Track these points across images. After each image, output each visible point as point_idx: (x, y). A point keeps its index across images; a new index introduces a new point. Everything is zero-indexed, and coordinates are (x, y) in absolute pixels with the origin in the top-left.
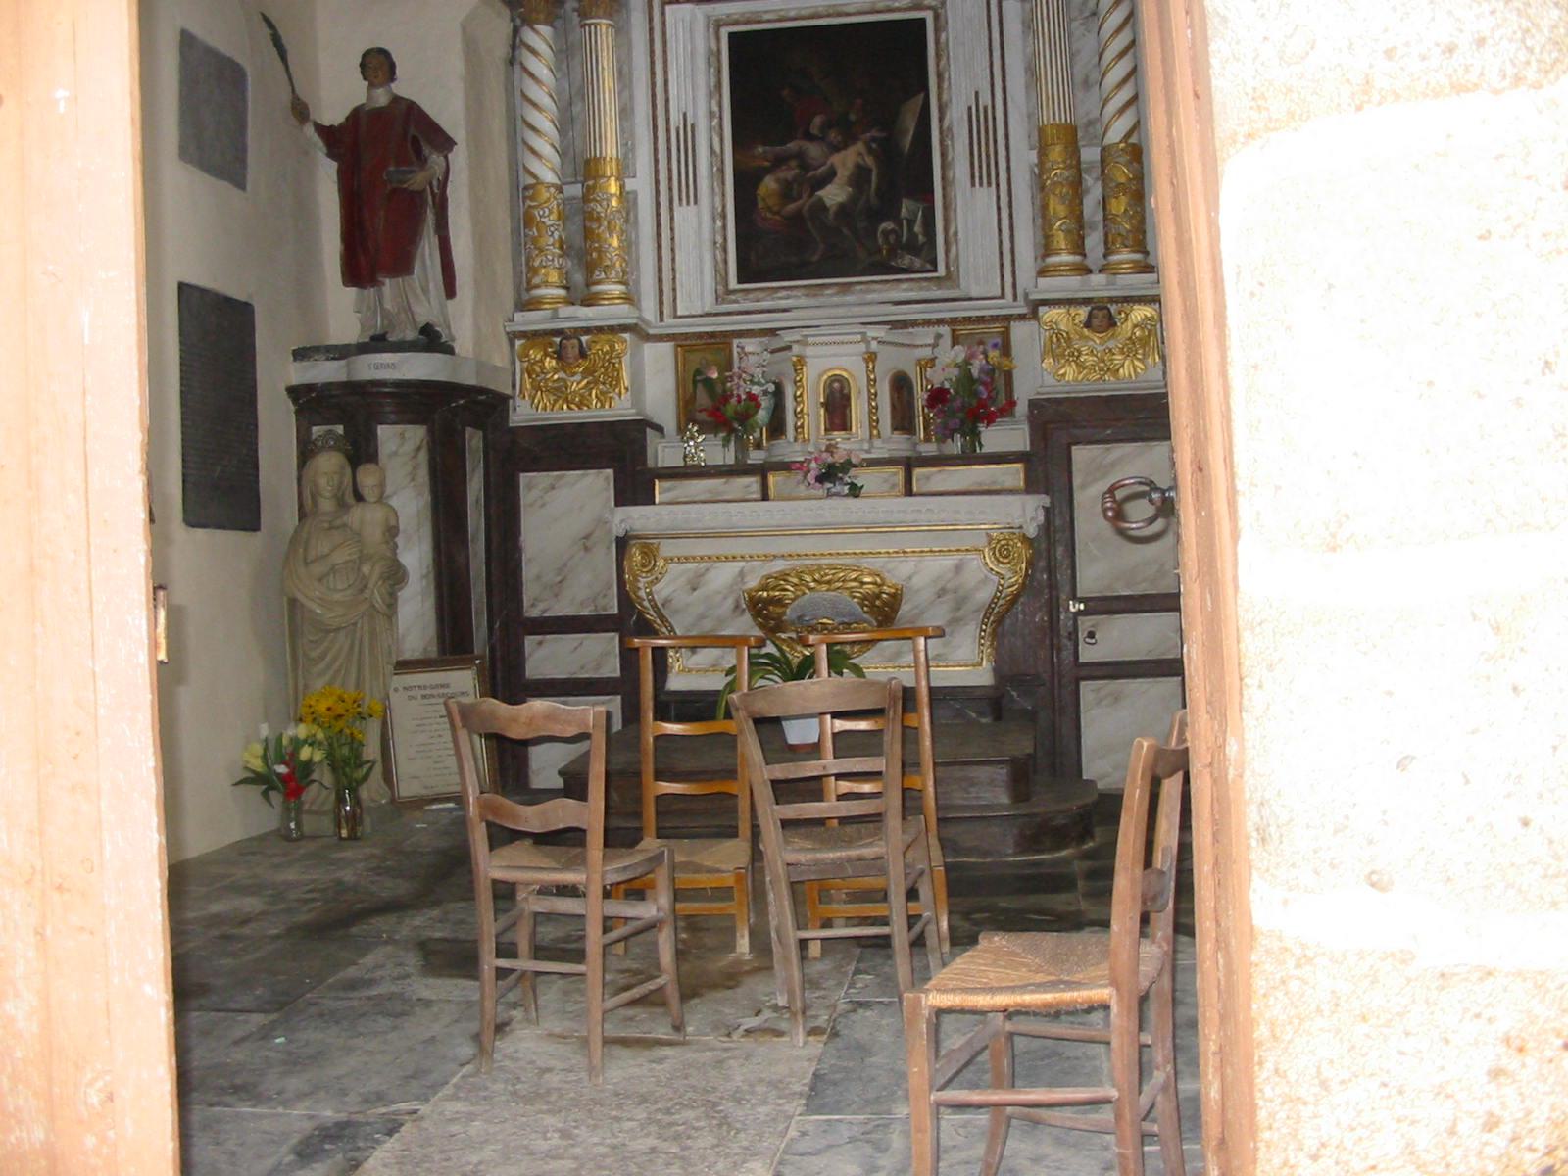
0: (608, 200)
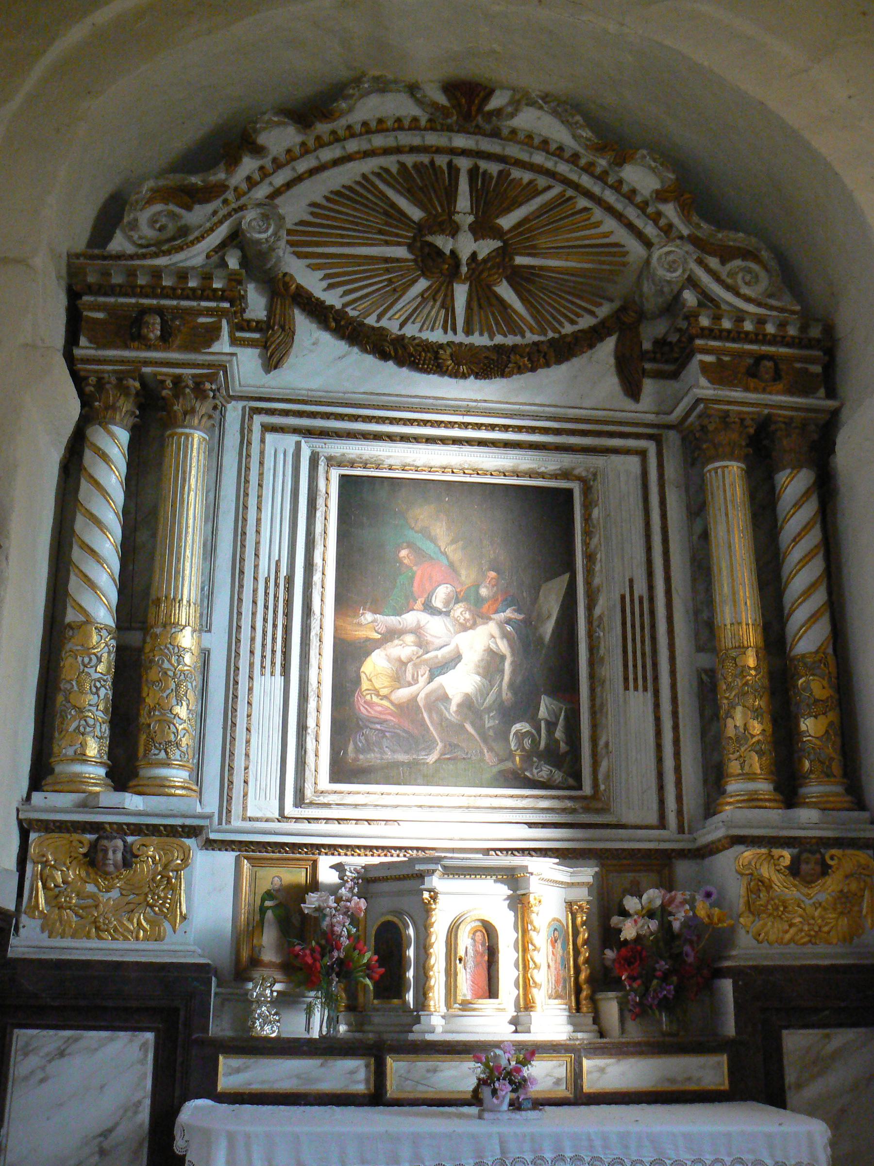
0: (180, 657)
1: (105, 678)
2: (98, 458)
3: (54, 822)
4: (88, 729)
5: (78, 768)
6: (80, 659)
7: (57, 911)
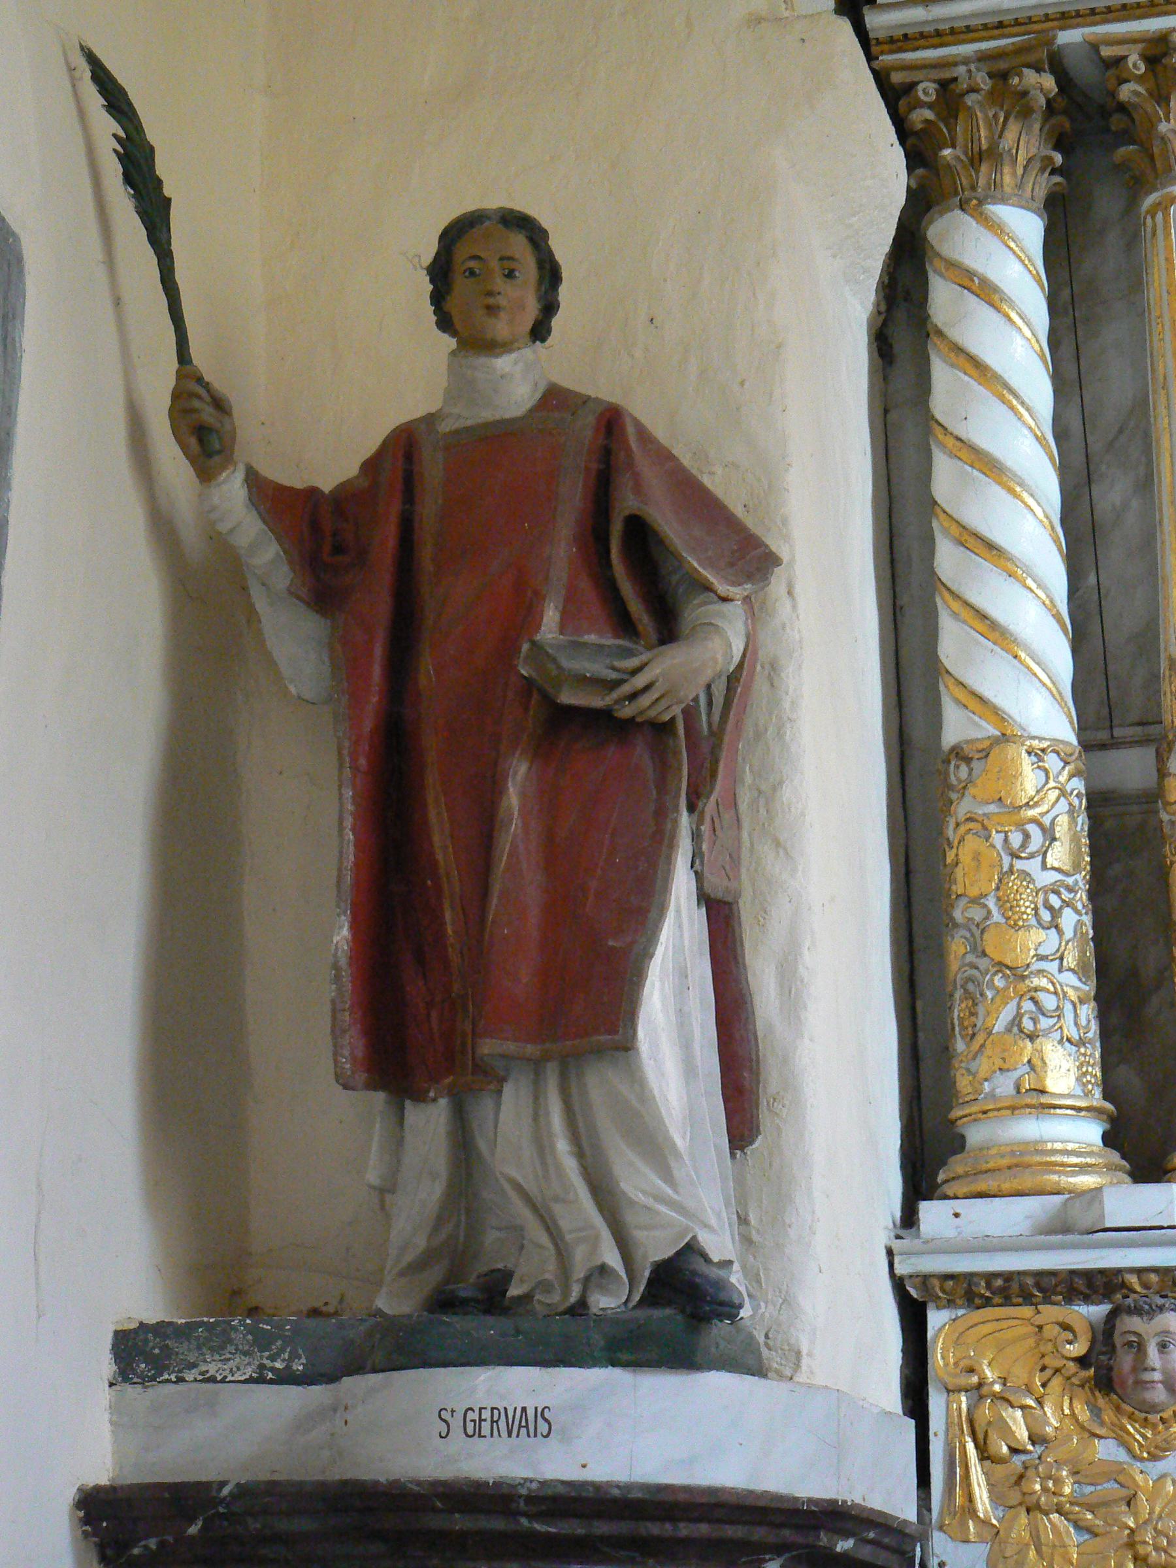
1: (1070, 881)
2: (973, 299)
3: (990, 1277)
4: (1045, 1023)
5: (1028, 1128)
6: (997, 839)
7: (1023, 1519)
